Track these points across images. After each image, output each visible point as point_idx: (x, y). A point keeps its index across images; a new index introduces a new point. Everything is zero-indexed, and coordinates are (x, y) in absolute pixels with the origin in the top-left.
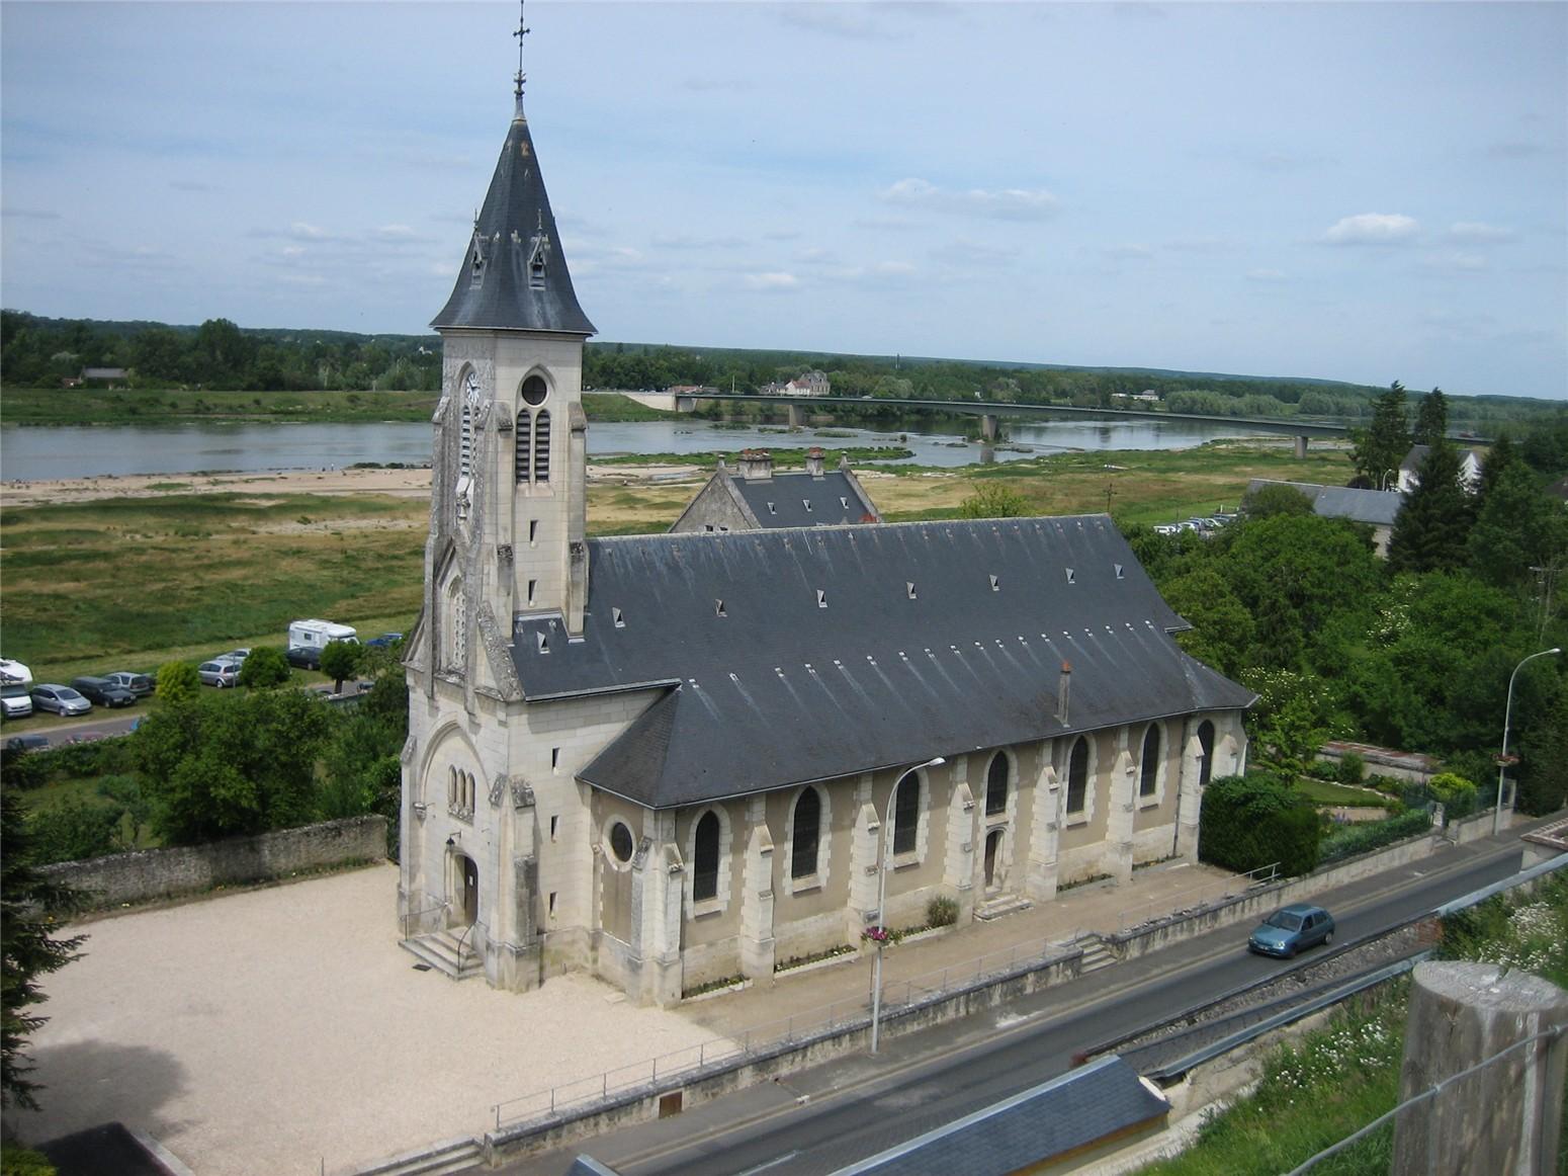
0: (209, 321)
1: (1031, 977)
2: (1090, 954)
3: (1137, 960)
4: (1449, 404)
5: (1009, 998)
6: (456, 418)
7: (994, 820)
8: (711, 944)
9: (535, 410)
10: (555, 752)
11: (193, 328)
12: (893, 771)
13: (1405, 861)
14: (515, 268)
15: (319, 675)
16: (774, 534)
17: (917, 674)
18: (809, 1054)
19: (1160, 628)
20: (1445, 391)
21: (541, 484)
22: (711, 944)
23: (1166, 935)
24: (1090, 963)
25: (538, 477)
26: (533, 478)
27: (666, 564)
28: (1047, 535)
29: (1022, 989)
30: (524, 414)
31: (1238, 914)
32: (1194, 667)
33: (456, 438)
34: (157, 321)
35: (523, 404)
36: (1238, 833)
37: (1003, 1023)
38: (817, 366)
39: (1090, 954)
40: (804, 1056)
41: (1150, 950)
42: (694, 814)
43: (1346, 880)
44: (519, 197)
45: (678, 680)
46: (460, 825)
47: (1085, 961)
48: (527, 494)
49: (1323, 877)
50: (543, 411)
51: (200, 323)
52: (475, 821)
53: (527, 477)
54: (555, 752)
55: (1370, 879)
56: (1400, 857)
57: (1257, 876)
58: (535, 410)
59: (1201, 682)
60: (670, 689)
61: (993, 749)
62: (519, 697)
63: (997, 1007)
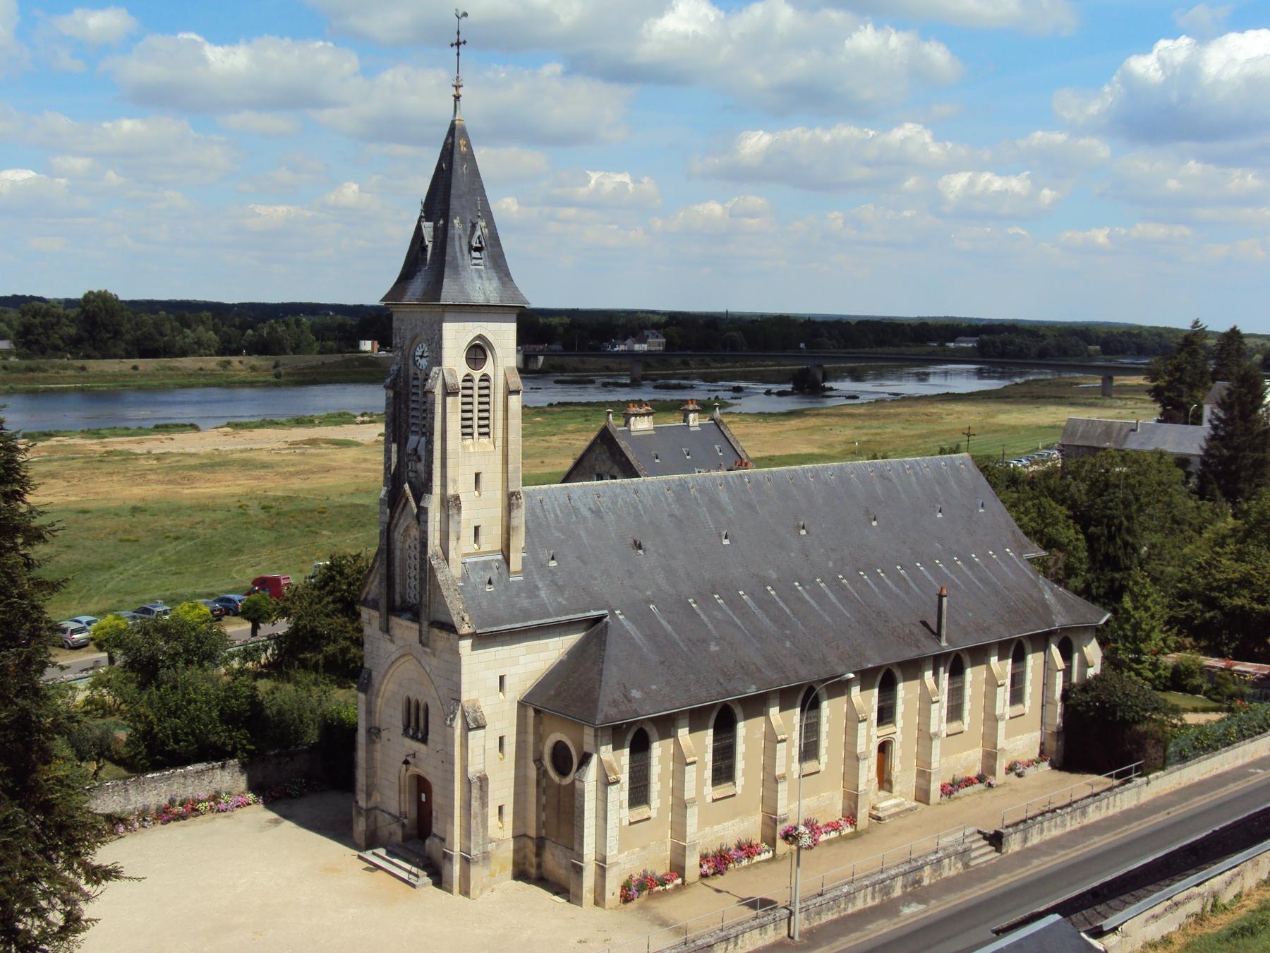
0: (91, 293)
1: (927, 870)
2: (976, 849)
3: (1017, 853)
4: (1246, 341)
5: (909, 889)
6: (407, 383)
7: (887, 730)
8: (644, 848)
9: (477, 375)
10: (502, 678)
11: (69, 303)
12: (875, 670)
13: (1248, 759)
14: (458, 249)
15: (236, 619)
16: (680, 479)
17: (812, 602)
18: (740, 942)
19: (1020, 555)
20: (1244, 329)
21: (484, 440)
22: (644, 848)
23: (1042, 831)
24: (976, 858)
25: (480, 434)
26: (476, 435)
27: (590, 509)
28: (916, 474)
29: (919, 882)
30: (469, 378)
31: (1104, 810)
32: (1052, 590)
33: (407, 401)
34: (20, 293)
35: (469, 370)
36: (1096, 738)
37: (907, 911)
38: (657, 326)
39: (976, 849)
40: (736, 944)
41: (1029, 844)
42: (710, 715)
43: (1197, 778)
44: (450, 189)
45: (605, 612)
46: (416, 746)
47: (973, 855)
48: (471, 449)
49: (1177, 774)
50: (485, 375)
51: (79, 295)
52: (429, 741)
53: (471, 434)
54: (502, 678)
55: (1219, 776)
56: (1243, 757)
57: (1118, 776)
58: (477, 375)
59: (1061, 605)
60: (599, 619)
61: (802, 685)
62: (471, 631)
63: (898, 898)
